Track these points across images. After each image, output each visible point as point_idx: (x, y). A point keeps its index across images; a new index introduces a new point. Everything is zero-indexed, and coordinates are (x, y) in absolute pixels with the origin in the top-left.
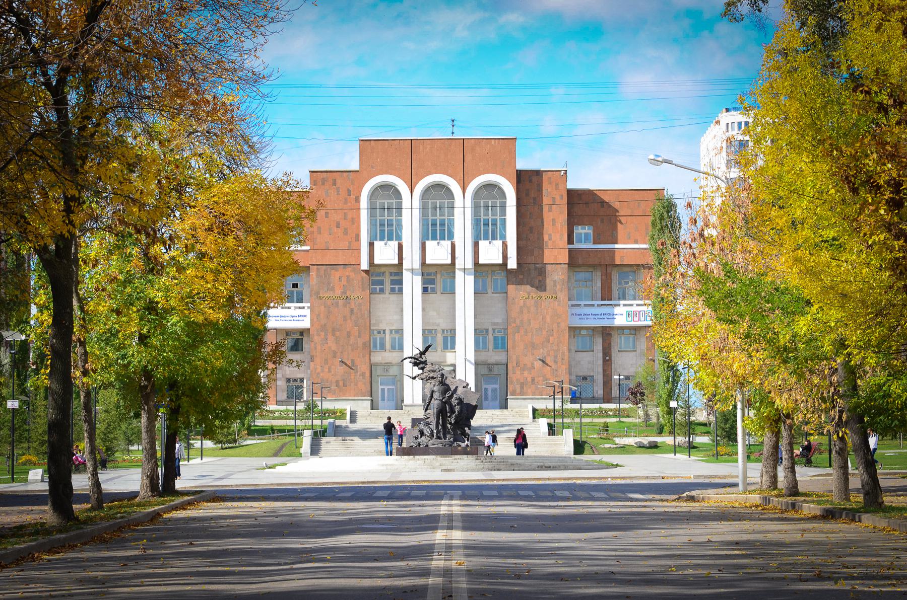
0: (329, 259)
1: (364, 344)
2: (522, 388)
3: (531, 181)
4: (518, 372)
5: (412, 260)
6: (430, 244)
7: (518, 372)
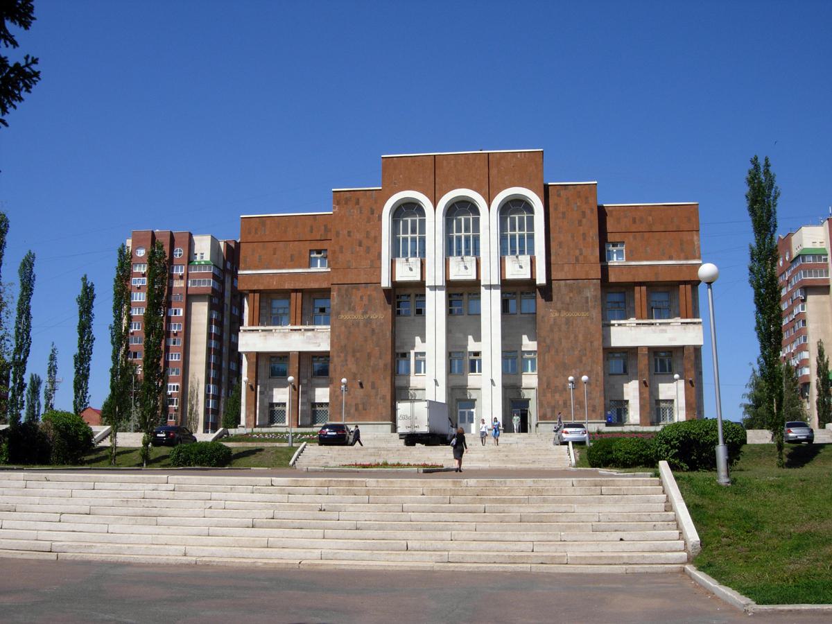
0: (351, 278)
2: (553, 411)
4: (549, 395)
5: (435, 276)
7: (549, 395)
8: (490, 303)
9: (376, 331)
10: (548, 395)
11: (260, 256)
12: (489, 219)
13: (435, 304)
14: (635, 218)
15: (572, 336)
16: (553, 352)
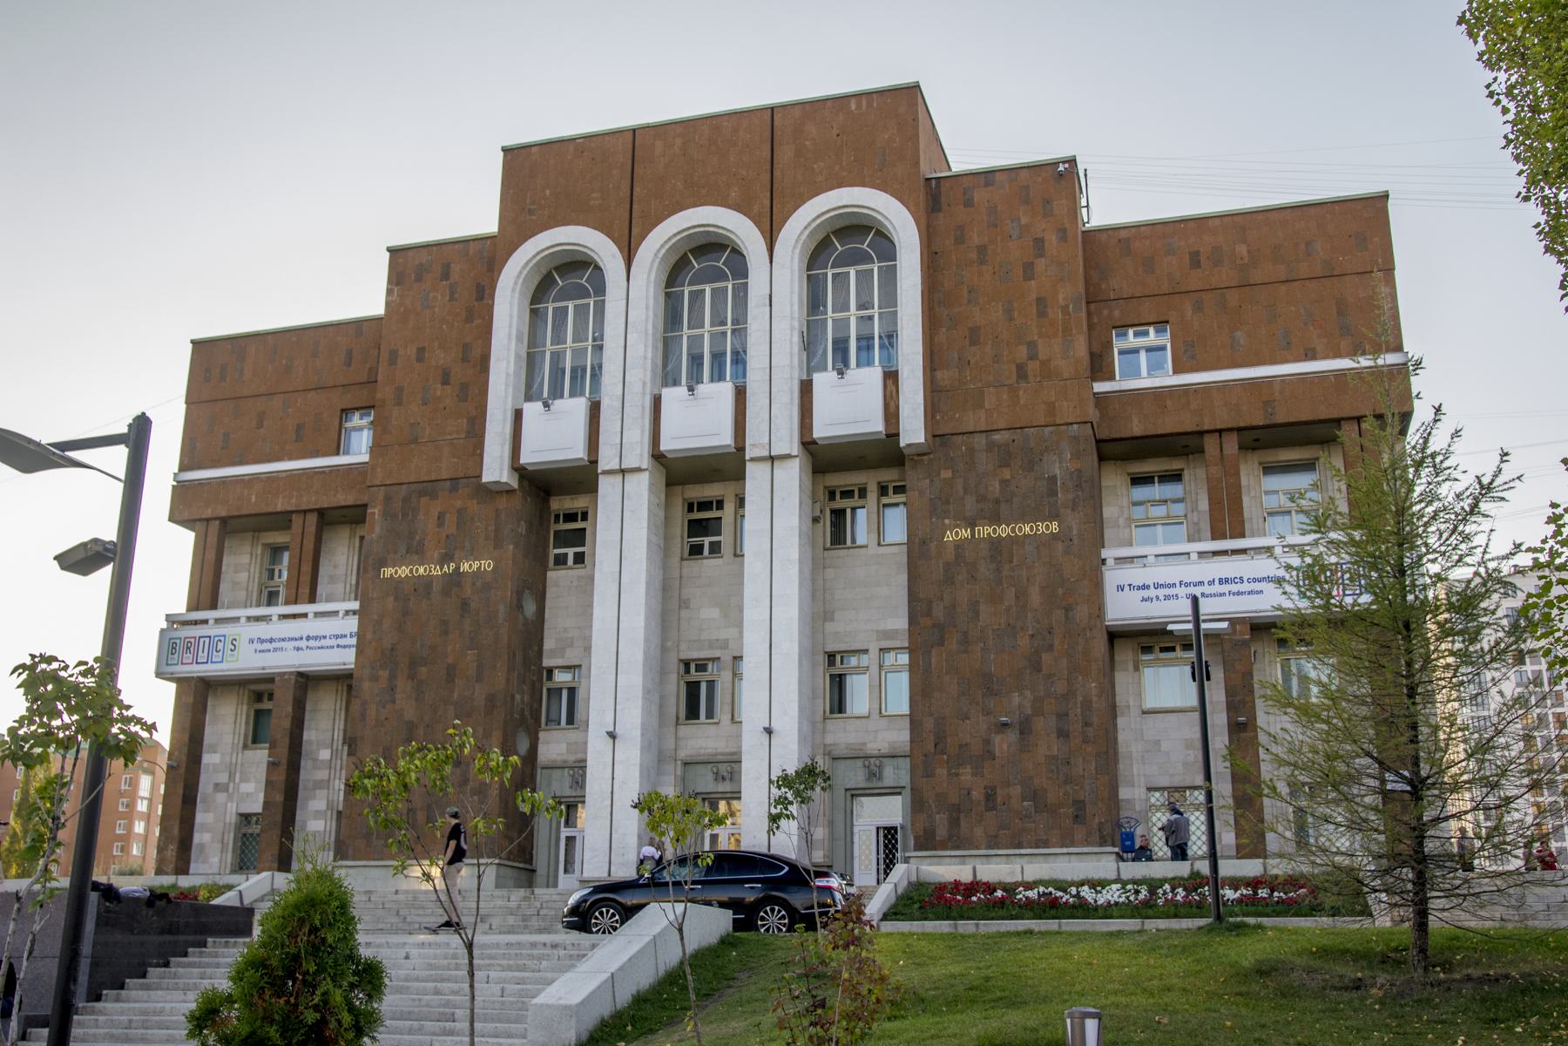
1: (491, 699)
2: (954, 823)
3: (969, 203)
4: (942, 772)
5: (625, 444)
6: (674, 397)
7: (942, 772)
8: (774, 509)
9: (473, 605)
10: (938, 771)
11: (226, 435)
12: (776, 278)
13: (626, 522)
14: (1197, 253)
15: (1010, 594)
16: (953, 644)
